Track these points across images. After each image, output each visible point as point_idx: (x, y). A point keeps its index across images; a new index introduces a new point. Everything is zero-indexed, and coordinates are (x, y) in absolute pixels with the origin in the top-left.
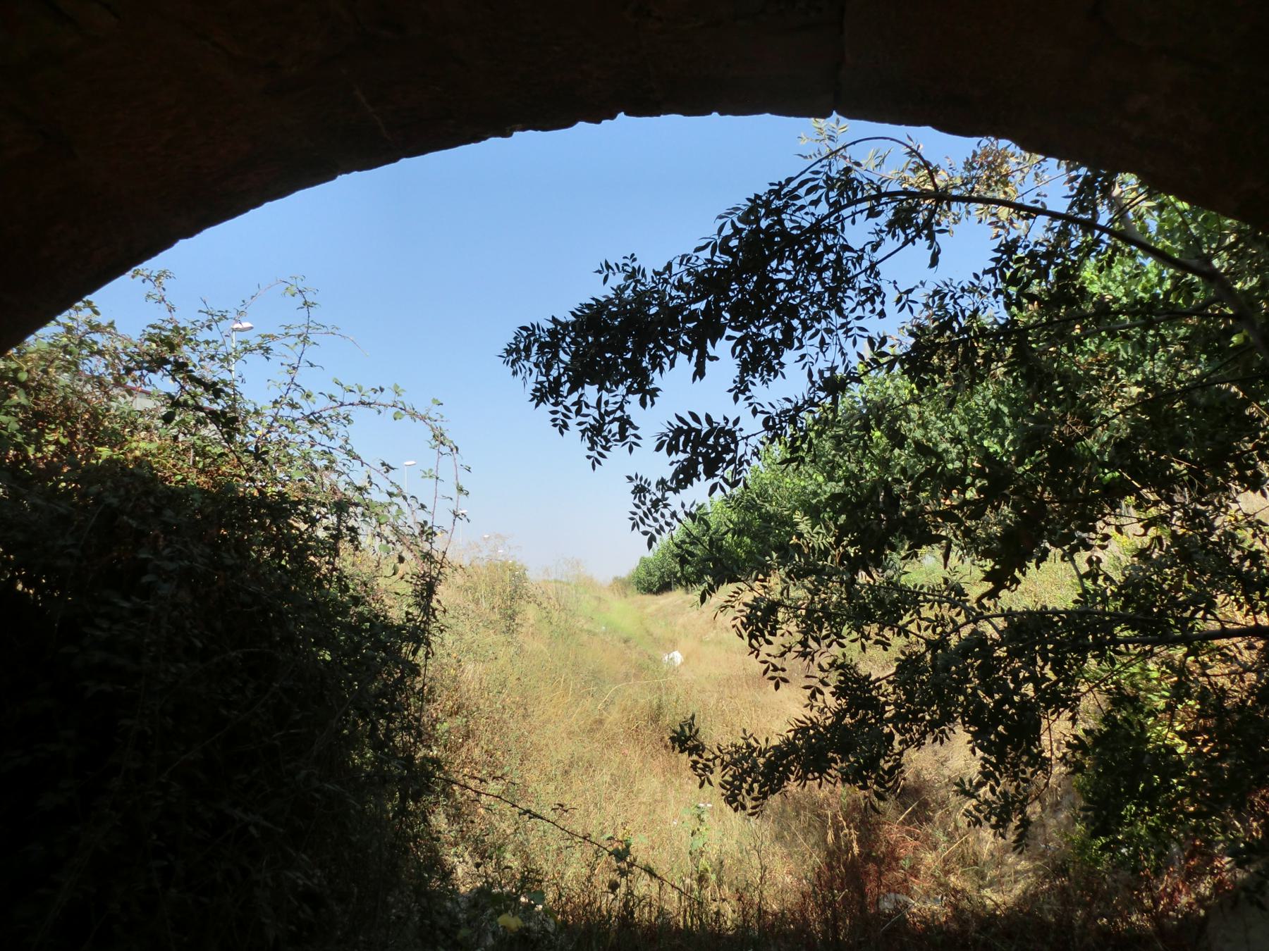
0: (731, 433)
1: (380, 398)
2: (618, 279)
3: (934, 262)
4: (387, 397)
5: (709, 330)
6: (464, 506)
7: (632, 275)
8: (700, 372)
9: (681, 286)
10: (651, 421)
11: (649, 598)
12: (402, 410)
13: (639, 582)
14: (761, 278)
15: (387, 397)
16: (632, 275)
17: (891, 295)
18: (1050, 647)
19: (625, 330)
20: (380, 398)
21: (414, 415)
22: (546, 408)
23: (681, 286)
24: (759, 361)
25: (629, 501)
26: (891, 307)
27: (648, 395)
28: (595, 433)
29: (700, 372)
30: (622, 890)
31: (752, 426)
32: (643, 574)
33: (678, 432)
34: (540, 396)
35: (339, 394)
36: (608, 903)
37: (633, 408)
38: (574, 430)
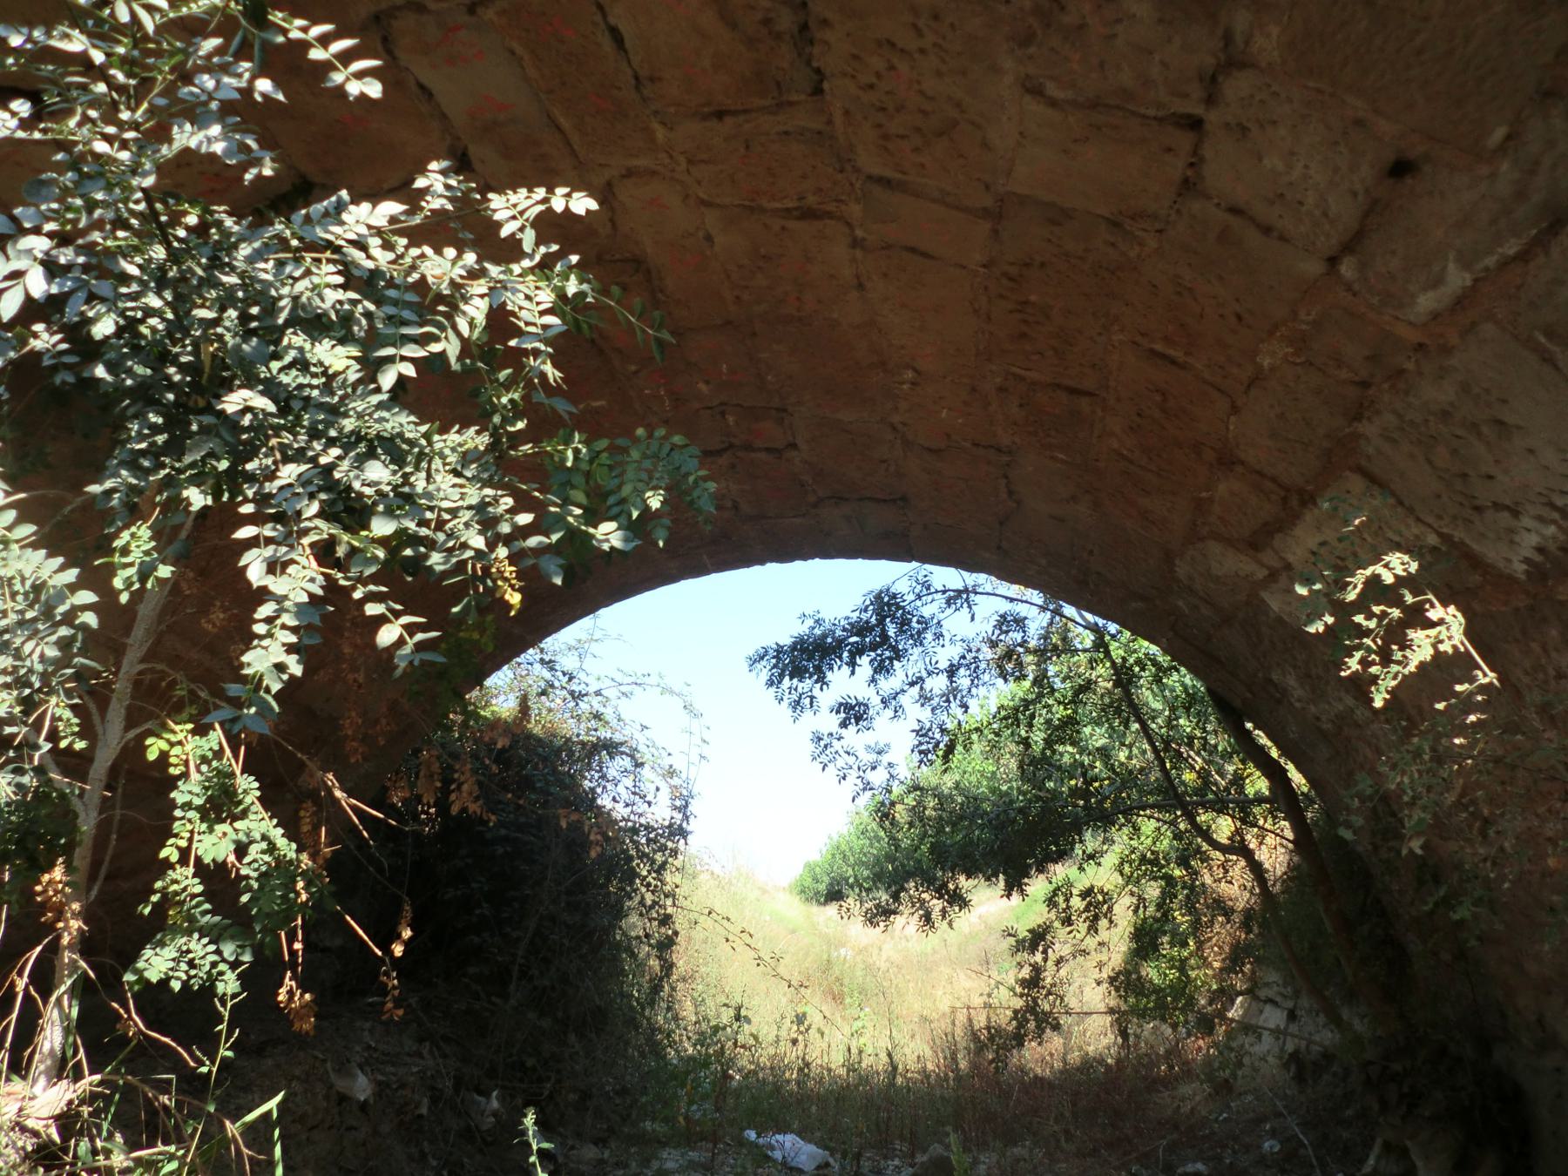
0: (866, 705)
1: (647, 680)
2: (810, 622)
3: (973, 619)
4: (653, 680)
5: (858, 651)
6: (705, 750)
7: (817, 621)
8: (853, 673)
9: (844, 630)
10: (828, 698)
11: (815, 909)
12: (667, 690)
13: (803, 892)
14: (881, 633)
15: (653, 680)
16: (817, 621)
17: (947, 637)
18: (255, 310)
19: (815, 650)
20: (647, 680)
21: (672, 692)
22: (774, 689)
23: (844, 630)
24: (881, 668)
25: (811, 747)
26: (947, 643)
27: (822, 680)
28: (796, 705)
29: (853, 673)
30: (801, 1046)
31: (875, 701)
32: (808, 882)
33: (841, 704)
34: (770, 683)
35: (619, 678)
36: (792, 1055)
37: (817, 691)
38: (785, 703)
